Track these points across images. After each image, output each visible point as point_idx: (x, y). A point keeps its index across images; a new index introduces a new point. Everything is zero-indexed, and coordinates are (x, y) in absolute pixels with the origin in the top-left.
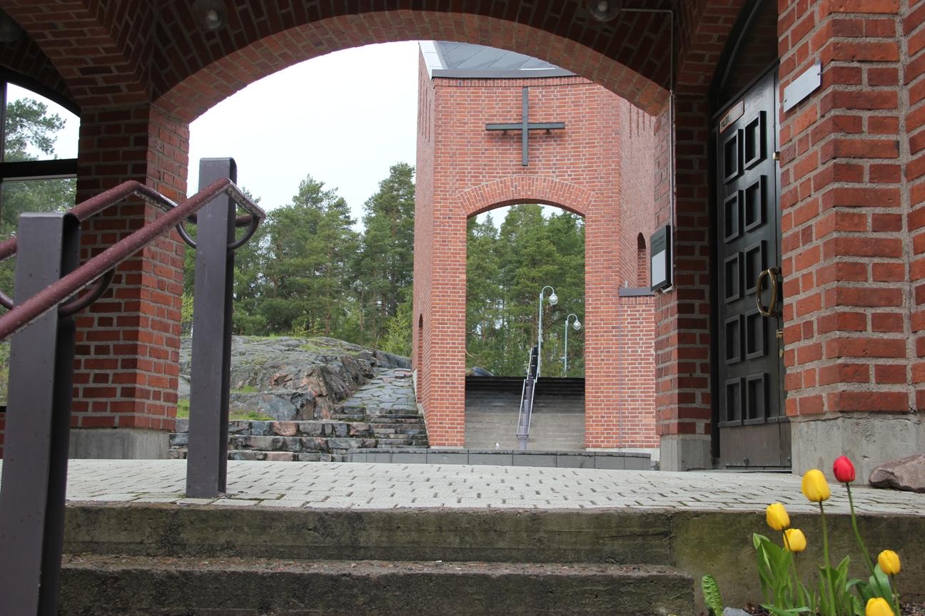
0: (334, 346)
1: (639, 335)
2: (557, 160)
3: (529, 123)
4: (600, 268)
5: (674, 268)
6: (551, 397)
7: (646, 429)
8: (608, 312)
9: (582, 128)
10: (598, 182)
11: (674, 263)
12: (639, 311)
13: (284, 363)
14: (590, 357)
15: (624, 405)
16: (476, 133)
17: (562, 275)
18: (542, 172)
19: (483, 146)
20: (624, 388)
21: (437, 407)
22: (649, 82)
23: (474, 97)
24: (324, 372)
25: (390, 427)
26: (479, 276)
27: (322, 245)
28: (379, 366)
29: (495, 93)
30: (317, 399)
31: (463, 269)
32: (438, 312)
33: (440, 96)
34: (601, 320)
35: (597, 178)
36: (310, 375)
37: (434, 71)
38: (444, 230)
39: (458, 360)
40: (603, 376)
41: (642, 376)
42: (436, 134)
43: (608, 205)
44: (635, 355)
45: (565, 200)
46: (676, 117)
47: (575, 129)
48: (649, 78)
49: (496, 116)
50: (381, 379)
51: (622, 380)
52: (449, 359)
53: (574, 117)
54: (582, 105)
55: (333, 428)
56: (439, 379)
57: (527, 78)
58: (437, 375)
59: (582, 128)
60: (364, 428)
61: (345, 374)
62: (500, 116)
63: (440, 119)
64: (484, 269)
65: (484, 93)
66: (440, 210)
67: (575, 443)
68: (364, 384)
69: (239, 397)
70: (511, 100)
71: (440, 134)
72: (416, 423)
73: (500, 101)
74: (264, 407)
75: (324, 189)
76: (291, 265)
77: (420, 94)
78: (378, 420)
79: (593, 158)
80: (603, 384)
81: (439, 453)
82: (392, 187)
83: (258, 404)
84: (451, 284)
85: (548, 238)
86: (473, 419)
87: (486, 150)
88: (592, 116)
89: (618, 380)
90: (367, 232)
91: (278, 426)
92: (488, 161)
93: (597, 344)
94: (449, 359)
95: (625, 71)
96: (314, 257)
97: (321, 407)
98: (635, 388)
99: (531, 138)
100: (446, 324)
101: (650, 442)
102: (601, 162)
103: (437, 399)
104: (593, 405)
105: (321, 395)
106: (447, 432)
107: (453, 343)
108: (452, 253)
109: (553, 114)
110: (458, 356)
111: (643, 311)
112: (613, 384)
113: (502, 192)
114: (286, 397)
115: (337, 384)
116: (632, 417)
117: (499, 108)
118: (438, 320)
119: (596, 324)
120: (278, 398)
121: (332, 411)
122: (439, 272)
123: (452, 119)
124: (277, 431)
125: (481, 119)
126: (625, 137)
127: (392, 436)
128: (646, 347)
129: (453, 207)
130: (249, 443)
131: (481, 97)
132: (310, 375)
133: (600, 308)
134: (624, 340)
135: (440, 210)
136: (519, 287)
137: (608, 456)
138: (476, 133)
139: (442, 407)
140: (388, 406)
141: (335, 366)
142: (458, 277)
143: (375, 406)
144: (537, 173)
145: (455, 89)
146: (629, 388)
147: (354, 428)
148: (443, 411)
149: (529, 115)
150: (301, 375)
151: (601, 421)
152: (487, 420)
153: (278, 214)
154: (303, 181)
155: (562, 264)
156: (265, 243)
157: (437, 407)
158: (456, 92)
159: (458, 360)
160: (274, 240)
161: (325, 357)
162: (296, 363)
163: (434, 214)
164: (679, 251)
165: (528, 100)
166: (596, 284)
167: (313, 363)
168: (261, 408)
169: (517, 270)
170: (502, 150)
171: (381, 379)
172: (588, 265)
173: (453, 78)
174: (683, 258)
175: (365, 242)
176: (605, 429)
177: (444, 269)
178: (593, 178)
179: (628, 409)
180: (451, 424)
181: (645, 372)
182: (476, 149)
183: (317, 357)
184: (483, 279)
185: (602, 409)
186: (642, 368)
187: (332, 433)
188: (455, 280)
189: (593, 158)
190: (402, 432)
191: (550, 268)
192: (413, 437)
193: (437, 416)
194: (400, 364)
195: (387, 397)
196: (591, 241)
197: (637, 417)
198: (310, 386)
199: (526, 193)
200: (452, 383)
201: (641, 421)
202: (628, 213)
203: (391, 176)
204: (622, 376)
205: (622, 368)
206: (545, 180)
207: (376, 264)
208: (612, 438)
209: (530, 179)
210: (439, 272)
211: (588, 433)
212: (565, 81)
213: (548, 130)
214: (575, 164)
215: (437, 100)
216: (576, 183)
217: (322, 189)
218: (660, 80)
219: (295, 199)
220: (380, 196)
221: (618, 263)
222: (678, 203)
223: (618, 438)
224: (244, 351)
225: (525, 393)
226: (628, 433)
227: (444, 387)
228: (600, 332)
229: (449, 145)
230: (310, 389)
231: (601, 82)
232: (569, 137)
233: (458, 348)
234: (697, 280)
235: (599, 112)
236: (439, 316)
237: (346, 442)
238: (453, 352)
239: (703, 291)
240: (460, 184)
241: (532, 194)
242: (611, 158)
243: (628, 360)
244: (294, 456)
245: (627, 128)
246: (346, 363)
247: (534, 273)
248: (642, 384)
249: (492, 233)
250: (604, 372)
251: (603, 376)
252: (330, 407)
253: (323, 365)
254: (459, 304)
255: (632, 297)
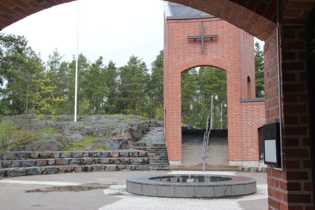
0: (136, 118)
1: (249, 117)
2: (215, 50)
3: (204, 36)
4: (233, 91)
5: (283, 155)
6: (215, 137)
7: (252, 154)
8: (236, 108)
9: (225, 37)
10: (232, 57)
11: (283, 152)
12: (248, 108)
13: (116, 127)
14: (229, 121)
15: (244, 144)
16: (184, 40)
17: (220, 87)
18: (209, 55)
19: (186, 45)
20: (243, 138)
21: (171, 146)
22: (261, 17)
23: (183, 26)
24: (131, 131)
25: (154, 153)
26: (190, 89)
27: (136, 79)
28: (152, 127)
29: (191, 24)
30: (128, 141)
31: (180, 93)
32: (171, 109)
33: (170, 26)
34: (234, 111)
35: (231, 56)
36: (125, 132)
37: (167, 17)
38: (172, 78)
39: (179, 128)
40: (235, 133)
41: (250, 133)
42: (168, 41)
43: (235, 67)
44: (247, 125)
45: (219, 65)
46: (282, 43)
47: (222, 37)
48: (261, 15)
49: (191, 33)
50: (152, 132)
51: (242, 135)
52: (175, 128)
53: (221, 33)
54: (224, 28)
55: (133, 153)
56: (172, 135)
57: (203, 18)
58: (171, 134)
59: (225, 37)
60: (144, 153)
61: (139, 131)
62: (193, 33)
63: (170, 35)
64: (192, 87)
65: (186, 25)
66: (170, 70)
67: (225, 158)
68: (146, 134)
69: (99, 141)
70: (197, 27)
71: (170, 41)
72: (164, 151)
73: (193, 27)
74: (108, 145)
75: (138, 59)
76: (126, 86)
77: (164, 26)
78: (150, 150)
79: (229, 48)
80: (235, 136)
81: (162, 185)
82: (161, 58)
83: (106, 144)
84: (175, 99)
85: (215, 74)
86: (186, 148)
87: (188, 46)
88: (229, 32)
89: (241, 135)
90: (152, 74)
91: (112, 154)
92: (189, 51)
93: (232, 121)
94: (175, 128)
95: (243, 10)
96: (134, 83)
97: (129, 144)
98: (248, 138)
99: (205, 41)
100: (174, 114)
101: (254, 159)
102: (232, 50)
103: (171, 143)
104: (231, 144)
105: (129, 140)
106: (175, 155)
107: (176, 121)
108: (175, 87)
109: (213, 32)
110: (178, 126)
111: (250, 107)
112: (239, 136)
113: (194, 63)
114: (116, 141)
115: (136, 135)
116: (247, 149)
117: (192, 30)
118: (171, 112)
119: (232, 113)
120: (113, 141)
121: (134, 145)
122: (171, 94)
123: (175, 35)
124: (112, 155)
125: (186, 35)
126: (242, 39)
127: (155, 156)
128: (251, 122)
129: (175, 69)
130: (100, 161)
131: (185, 26)
132: (125, 132)
133: (233, 107)
134: (243, 119)
135: (170, 70)
136: (205, 92)
137: (237, 185)
138: (184, 40)
139: (173, 146)
140: (154, 143)
141: (135, 128)
142: (178, 96)
143: (150, 143)
144: (208, 55)
145: (175, 24)
146: (245, 138)
147: (140, 153)
148: (173, 148)
149: (204, 32)
150: (122, 132)
151: (234, 151)
152: (191, 148)
153: (122, 68)
154: (131, 57)
155: (220, 83)
156: (118, 78)
157: (171, 146)
158: (176, 25)
159: (179, 128)
160: (121, 77)
161: (131, 124)
162: (120, 127)
163: (168, 72)
164: (287, 142)
165: (204, 27)
166: (231, 97)
167: (127, 127)
168: (107, 145)
169: (204, 86)
170: (194, 46)
171: (152, 132)
172: (228, 90)
173: (174, 20)
174: (290, 148)
175: (151, 77)
176: (236, 154)
177: (172, 93)
178: (229, 56)
179: (245, 146)
180: (177, 152)
181: (251, 131)
182: (184, 47)
183: (129, 124)
184: (191, 91)
185: (235, 146)
186: (250, 130)
187: (132, 155)
188: (177, 97)
189: (229, 48)
190: (159, 155)
191: (216, 85)
192: (163, 157)
193: (171, 149)
194: (159, 126)
195: (154, 139)
196: (229, 81)
197: (249, 149)
198: (125, 136)
199: (204, 63)
200: (177, 137)
201: (250, 151)
202: (244, 69)
203: (160, 54)
204: (242, 133)
205: (242, 130)
206: (211, 57)
207: (155, 85)
208: (239, 157)
209: (205, 57)
210: (171, 94)
211: (229, 155)
212: (212, 19)
213: (211, 38)
214: (223, 51)
215: (168, 28)
216: (222, 58)
217: (137, 59)
218: (268, 16)
219: (128, 63)
220: (157, 61)
221: (240, 89)
222: (284, 106)
223: (241, 157)
224: (103, 122)
225: (205, 138)
226: (245, 155)
227: (173, 138)
228: (233, 116)
229: (174, 45)
230: (125, 137)
231: (226, 19)
232: (220, 40)
233: (178, 123)
234: (301, 164)
235: (231, 30)
236: (171, 111)
237: (137, 159)
238: (177, 125)
239: (307, 173)
240: (178, 60)
241: (206, 63)
242: (236, 48)
243: (244, 127)
244: (117, 167)
245: (242, 36)
246: (139, 126)
247: (210, 87)
248: (250, 136)
249: (195, 73)
250: (235, 132)
251: (235, 133)
252: (133, 144)
253: (130, 127)
254: (179, 106)
255: (246, 102)
